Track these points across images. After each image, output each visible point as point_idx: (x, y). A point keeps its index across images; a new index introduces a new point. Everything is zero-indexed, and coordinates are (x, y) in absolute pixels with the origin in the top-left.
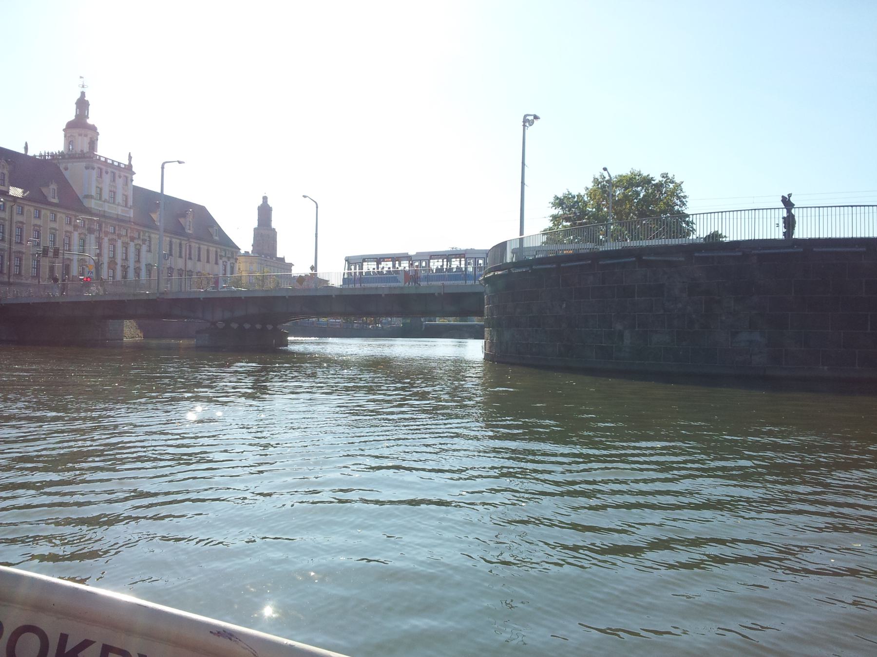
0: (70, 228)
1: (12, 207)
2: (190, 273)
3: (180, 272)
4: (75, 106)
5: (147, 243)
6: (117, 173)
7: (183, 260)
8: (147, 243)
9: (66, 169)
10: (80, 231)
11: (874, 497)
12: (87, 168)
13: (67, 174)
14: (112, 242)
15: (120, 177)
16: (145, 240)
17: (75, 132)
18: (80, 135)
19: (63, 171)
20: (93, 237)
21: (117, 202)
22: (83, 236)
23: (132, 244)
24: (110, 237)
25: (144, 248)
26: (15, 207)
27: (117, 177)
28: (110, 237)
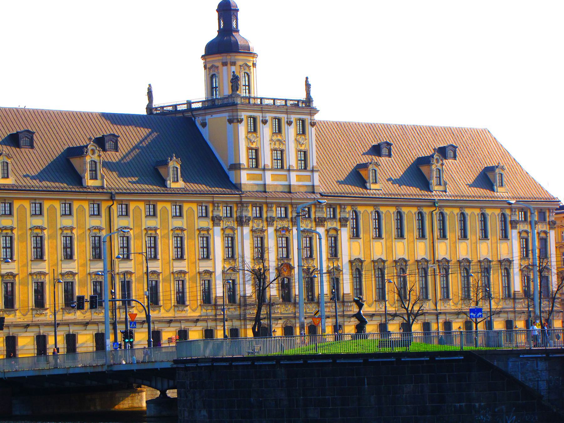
0: (205, 223)
1: (110, 208)
2: (444, 266)
3: (423, 267)
4: (216, 14)
5: (350, 223)
6: (284, 117)
7: (428, 241)
8: (350, 223)
9: (204, 125)
10: (223, 224)
11: (63, 159)
12: (230, 121)
13: (205, 132)
14: (283, 232)
15: (289, 123)
16: (346, 220)
17: (217, 59)
18: (225, 64)
19: (200, 128)
20: (246, 230)
21: (261, 166)
22: (228, 232)
23: (321, 230)
24: (279, 224)
25: (345, 234)
26: (114, 207)
27: (284, 126)
28: (279, 224)
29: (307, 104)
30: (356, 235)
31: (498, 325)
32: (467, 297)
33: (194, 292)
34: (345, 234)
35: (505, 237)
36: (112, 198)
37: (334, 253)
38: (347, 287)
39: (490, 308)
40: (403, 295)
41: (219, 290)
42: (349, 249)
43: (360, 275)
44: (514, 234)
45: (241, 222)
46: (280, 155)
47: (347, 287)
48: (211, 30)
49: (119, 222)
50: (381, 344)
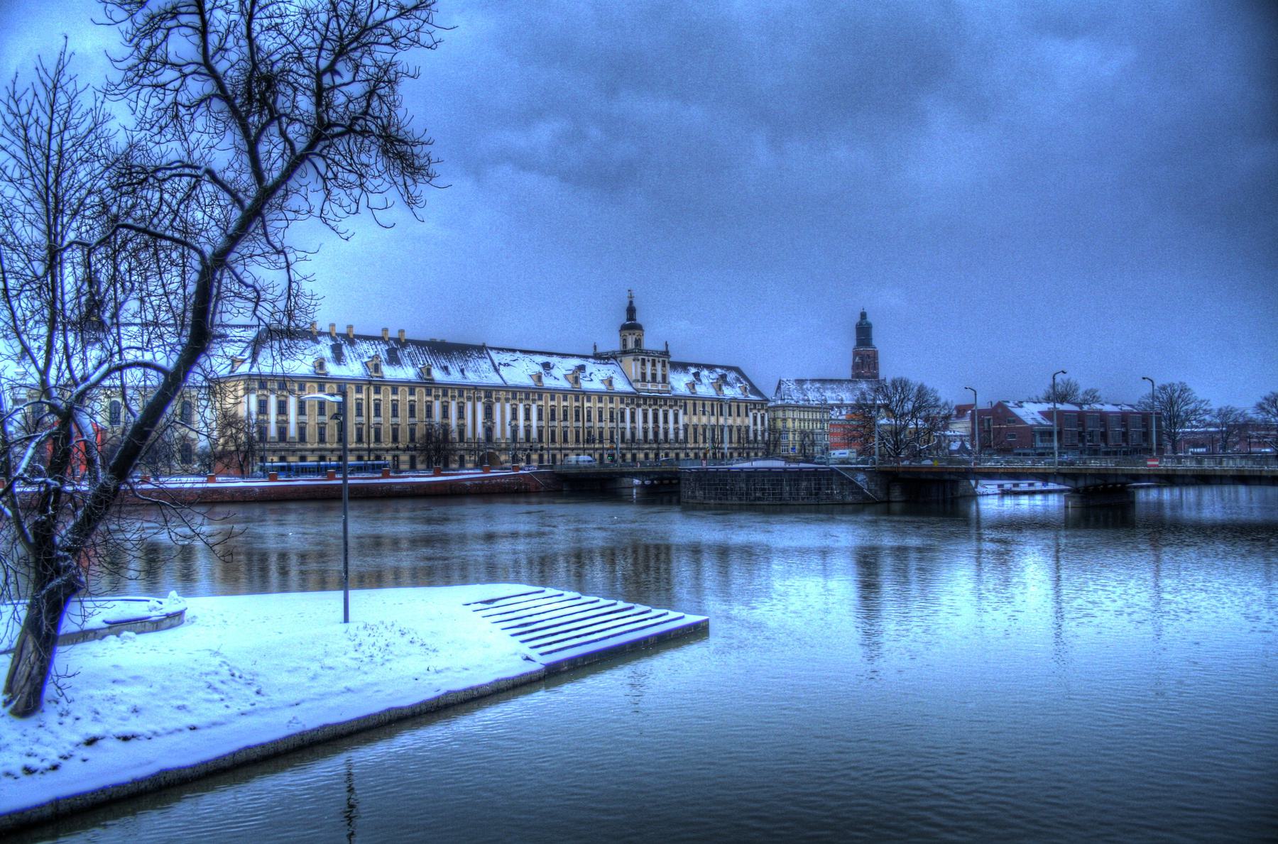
17: (626, 333)
29: (666, 353)
30: (685, 413)
31: (672, 455)
32: (739, 442)
33: (617, 437)
34: (681, 412)
35: (747, 415)
36: (283, 386)
37: (676, 421)
38: (681, 435)
39: (489, 430)
40: (713, 440)
41: (628, 435)
42: (682, 419)
43: (340, 435)
44: (751, 414)
45: (638, 406)
46: (654, 376)
47: (681, 435)
48: (623, 319)
49: (587, 404)
50: (540, 467)
